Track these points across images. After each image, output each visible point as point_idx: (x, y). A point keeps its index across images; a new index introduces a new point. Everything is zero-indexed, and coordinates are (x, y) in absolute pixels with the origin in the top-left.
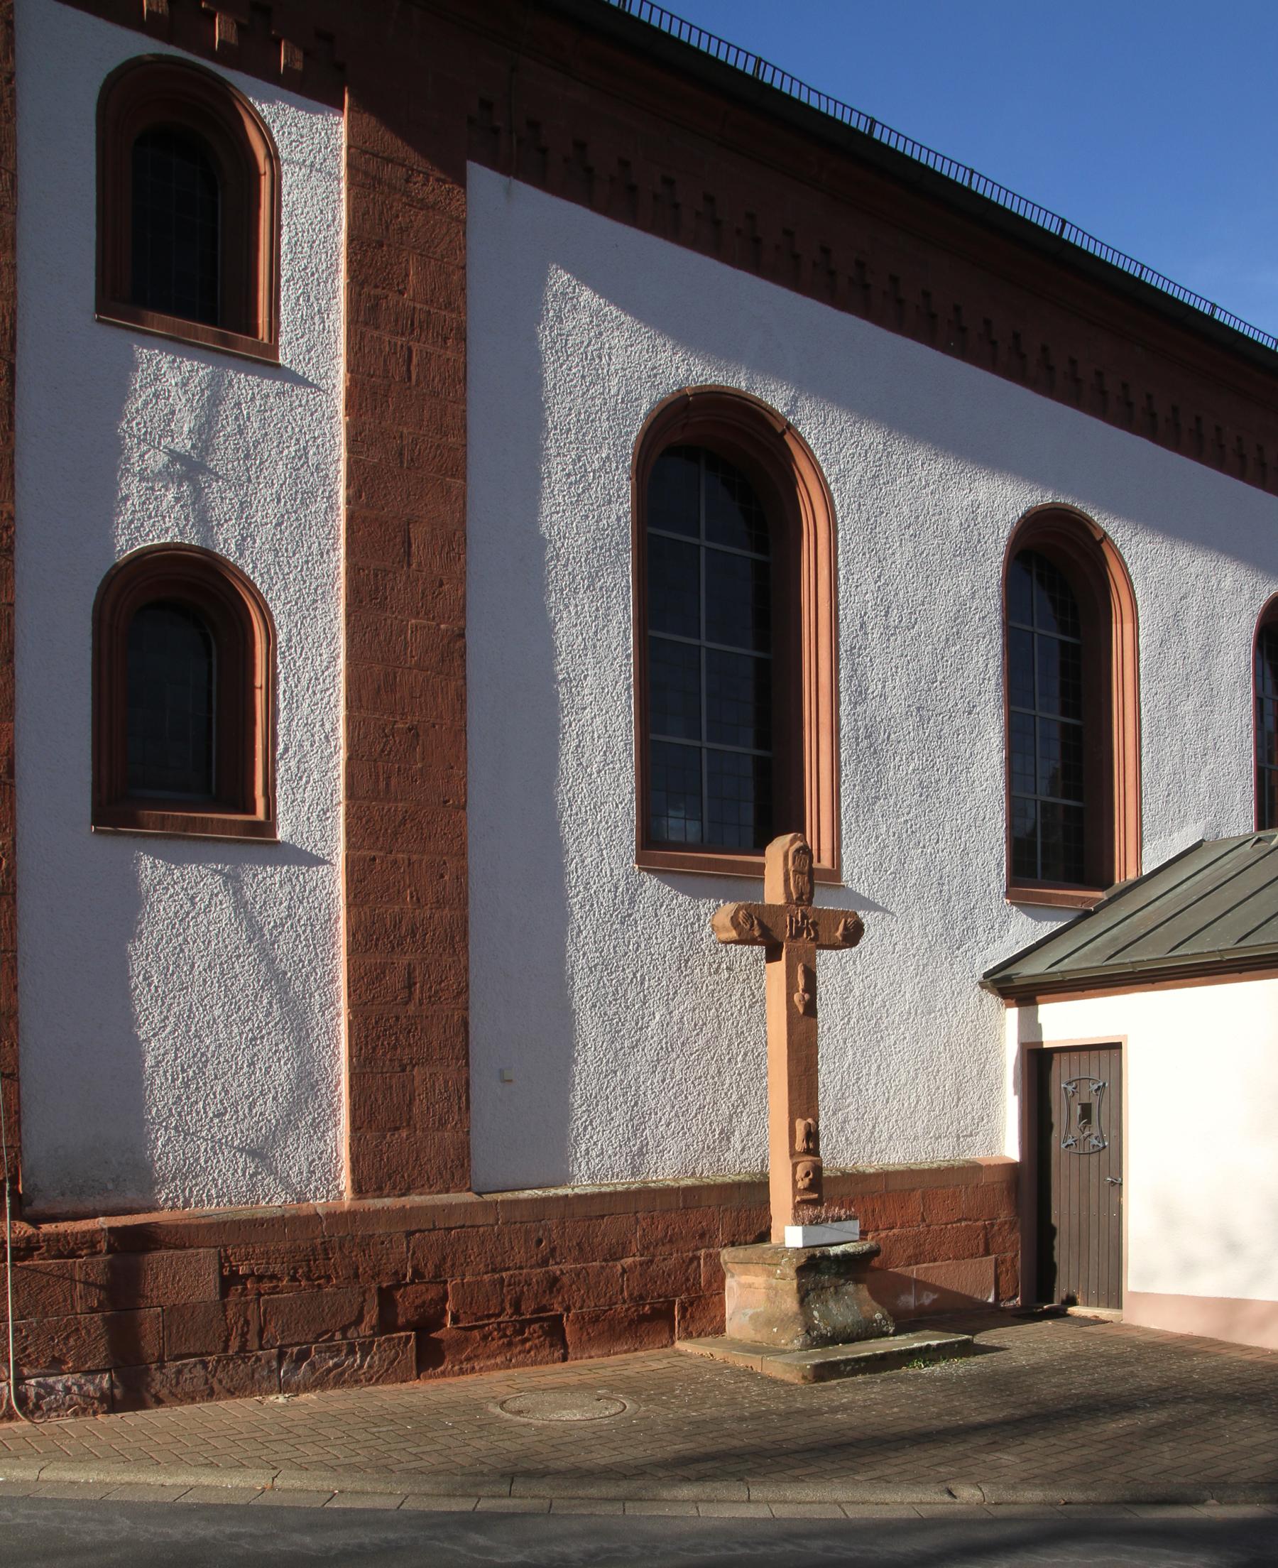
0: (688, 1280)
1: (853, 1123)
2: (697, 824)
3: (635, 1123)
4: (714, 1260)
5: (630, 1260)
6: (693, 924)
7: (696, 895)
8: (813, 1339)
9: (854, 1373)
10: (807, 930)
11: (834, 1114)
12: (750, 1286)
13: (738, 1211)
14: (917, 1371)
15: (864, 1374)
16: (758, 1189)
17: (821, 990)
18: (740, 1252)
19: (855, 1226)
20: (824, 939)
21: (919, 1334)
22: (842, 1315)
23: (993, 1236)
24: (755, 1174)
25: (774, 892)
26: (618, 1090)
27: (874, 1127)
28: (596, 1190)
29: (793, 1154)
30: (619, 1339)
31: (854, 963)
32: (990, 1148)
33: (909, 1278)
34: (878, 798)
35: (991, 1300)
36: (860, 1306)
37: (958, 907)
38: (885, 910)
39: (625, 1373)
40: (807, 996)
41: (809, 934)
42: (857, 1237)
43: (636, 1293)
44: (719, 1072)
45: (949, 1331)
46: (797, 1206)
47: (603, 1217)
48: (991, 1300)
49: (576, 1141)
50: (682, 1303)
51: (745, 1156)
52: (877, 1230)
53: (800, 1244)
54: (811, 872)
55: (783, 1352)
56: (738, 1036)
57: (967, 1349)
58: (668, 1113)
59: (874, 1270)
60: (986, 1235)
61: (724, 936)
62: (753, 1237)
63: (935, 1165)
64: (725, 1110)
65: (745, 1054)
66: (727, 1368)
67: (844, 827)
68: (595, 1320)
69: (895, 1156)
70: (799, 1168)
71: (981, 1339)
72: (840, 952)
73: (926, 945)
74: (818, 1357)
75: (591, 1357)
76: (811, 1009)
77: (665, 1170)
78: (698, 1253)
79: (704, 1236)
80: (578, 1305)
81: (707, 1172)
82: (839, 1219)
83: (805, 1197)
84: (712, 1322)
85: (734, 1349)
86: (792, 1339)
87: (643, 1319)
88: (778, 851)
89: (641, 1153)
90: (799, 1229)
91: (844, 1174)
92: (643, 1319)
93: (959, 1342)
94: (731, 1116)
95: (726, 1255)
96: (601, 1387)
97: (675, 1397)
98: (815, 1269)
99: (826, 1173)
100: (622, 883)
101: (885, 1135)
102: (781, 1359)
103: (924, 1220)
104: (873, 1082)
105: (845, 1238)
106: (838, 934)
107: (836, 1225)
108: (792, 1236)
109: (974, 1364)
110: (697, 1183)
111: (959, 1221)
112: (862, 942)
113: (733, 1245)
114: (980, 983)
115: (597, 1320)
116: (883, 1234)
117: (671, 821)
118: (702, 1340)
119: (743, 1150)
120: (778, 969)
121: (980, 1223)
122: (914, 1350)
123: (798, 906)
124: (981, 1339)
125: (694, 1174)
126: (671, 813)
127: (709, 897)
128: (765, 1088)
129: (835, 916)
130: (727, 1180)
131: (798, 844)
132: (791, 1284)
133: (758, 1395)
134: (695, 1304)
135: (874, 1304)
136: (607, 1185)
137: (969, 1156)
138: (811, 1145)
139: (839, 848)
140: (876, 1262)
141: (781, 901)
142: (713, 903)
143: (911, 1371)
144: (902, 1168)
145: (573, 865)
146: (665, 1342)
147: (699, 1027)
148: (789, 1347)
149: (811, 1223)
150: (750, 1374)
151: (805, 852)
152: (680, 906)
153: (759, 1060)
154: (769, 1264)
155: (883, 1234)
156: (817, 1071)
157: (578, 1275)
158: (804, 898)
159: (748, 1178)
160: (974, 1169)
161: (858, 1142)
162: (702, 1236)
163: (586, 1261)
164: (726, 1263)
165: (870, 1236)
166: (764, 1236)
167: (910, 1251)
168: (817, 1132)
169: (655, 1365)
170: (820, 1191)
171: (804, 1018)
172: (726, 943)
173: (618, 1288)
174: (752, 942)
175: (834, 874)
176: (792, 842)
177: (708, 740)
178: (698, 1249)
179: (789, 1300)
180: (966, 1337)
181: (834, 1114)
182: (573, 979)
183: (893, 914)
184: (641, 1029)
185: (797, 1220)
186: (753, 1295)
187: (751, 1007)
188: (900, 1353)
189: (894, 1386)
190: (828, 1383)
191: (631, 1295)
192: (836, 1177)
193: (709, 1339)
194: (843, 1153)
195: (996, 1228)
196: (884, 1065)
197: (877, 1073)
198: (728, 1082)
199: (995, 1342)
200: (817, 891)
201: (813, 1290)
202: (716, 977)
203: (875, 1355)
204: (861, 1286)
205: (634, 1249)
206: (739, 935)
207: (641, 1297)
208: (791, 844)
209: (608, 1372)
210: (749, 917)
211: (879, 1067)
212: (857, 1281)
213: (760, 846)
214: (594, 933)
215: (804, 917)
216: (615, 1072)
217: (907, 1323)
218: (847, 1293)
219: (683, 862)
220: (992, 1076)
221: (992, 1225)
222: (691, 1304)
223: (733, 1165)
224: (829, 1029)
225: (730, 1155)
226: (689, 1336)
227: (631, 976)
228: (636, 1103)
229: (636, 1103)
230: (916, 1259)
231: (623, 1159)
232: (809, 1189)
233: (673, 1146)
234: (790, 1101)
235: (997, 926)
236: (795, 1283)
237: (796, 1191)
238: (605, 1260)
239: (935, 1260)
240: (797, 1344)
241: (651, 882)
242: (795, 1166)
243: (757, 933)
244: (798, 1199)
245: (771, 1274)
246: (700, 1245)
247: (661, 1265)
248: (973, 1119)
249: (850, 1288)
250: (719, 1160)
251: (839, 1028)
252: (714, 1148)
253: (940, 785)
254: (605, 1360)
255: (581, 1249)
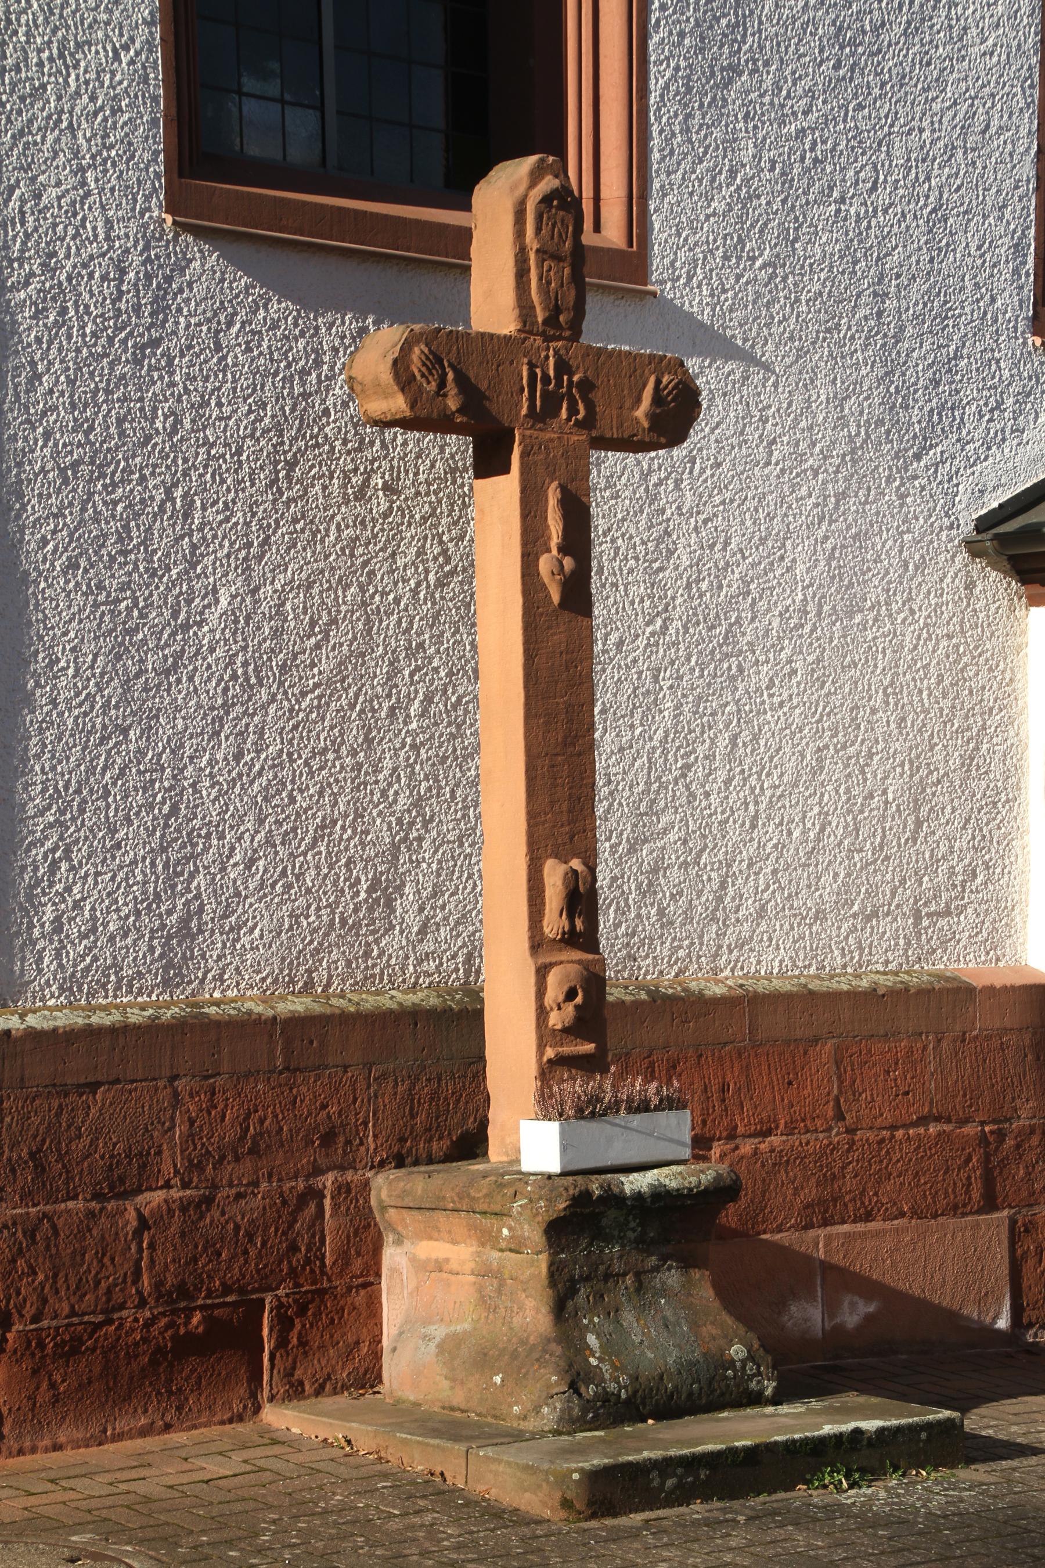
0: (294, 1248)
1: (675, 874)
2: (312, 117)
3: (173, 857)
4: (355, 1199)
5: (157, 1197)
6: (304, 372)
7: (311, 301)
8: (587, 1405)
9: (683, 1496)
10: (565, 401)
11: (632, 850)
12: (439, 1266)
13: (419, 1078)
14: (831, 1496)
15: (706, 1498)
16: (455, 1026)
17: (601, 550)
18: (417, 1182)
19: (678, 1126)
20: (607, 427)
21: (834, 1401)
22: (653, 1347)
23: (1003, 1163)
24: (452, 991)
25: (492, 303)
26: (133, 777)
27: (723, 885)
28: (79, 1020)
29: (537, 943)
30: (127, 1398)
32: (993, 945)
33: (808, 1259)
34: (735, 70)
35: (1003, 1323)
36: (694, 1326)
37: (919, 354)
38: (748, 358)
39: (140, 1487)
40: (568, 563)
41: (573, 411)
42: (686, 1153)
43: (170, 1281)
44: (369, 741)
45: (904, 1397)
46: (547, 1071)
47: (93, 1087)
48: (1003, 1323)
49: (30, 897)
50: (279, 1307)
51: (428, 946)
52: (732, 1136)
53: (555, 1168)
54: (579, 252)
55: (517, 1437)
56: (411, 653)
57: (949, 1447)
58: (250, 837)
59: (728, 1235)
60: (987, 1159)
61: (378, 407)
62: (446, 1143)
63: (864, 983)
64: (381, 831)
65: (428, 699)
66: (385, 1476)
67: (656, 142)
68: (71, 1349)
69: (769, 954)
70: (553, 978)
71: (984, 1421)
72: (645, 458)
73: (843, 448)
74: (598, 1451)
75: (57, 1447)
76: (577, 595)
77: (244, 976)
78: (319, 1182)
79: (333, 1140)
80: (29, 1311)
81: (343, 983)
82: (644, 1107)
83: (567, 1050)
84: (349, 1355)
85: (400, 1426)
86: (535, 1402)
87: (188, 1346)
88: (500, 201)
89: (186, 932)
90: (553, 1128)
91: (655, 995)
92: (188, 1346)
93: (929, 1426)
94: (395, 848)
95: (385, 1187)
96: (79, 1527)
97: (259, 1552)
98: (594, 1231)
99: (614, 994)
100: (135, 259)
101: (749, 907)
102: (512, 1454)
103: (840, 1116)
104: (722, 775)
105: (658, 1153)
106: (641, 412)
107: (637, 1120)
108: (536, 1145)
109: (970, 1483)
110: (317, 1009)
111: (923, 1121)
112: (695, 436)
113: (400, 1165)
114: (968, 543)
115: (75, 1351)
116: (747, 1147)
117: (250, 106)
118: (327, 1402)
119: (423, 931)
120: (500, 497)
121: (971, 1130)
122: (822, 1440)
123: (548, 339)
124: (984, 1421)
125: (309, 985)
126: (249, 84)
127: (341, 308)
128: (474, 783)
129: (636, 366)
130: (386, 1002)
131: (548, 183)
132: (534, 1265)
133: (458, 1547)
134: (304, 1313)
135: (729, 1320)
136: (104, 1008)
137: (945, 964)
138: (579, 924)
140: (730, 1216)
141: (506, 325)
142: (349, 323)
143: (817, 1497)
144: (786, 986)
145: (14, 204)
146: (237, 1407)
147: (321, 628)
148: (531, 1425)
149: (580, 1114)
150: (437, 1491)
151: (563, 205)
152: (275, 326)
153: (461, 714)
154: (483, 1212)
155: (747, 1147)
156: (591, 746)
157: (31, 1234)
158: (559, 318)
159: (434, 1001)
160: (957, 994)
161: (688, 919)
162: (328, 1139)
163: (52, 1198)
164: (384, 1208)
165: (715, 1152)
166: (472, 1144)
167: (810, 1192)
168: (593, 893)
169: (214, 1468)
170: (602, 1037)
171: (562, 613)
172: (384, 424)
173: (128, 1267)
174: (441, 424)
175: (633, 262)
176: (535, 176)
178: (318, 1171)
179: (530, 1303)
180: (946, 1414)
181: (632, 850)
182: (20, 496)
183: (767, 367)
184: (186, 627)
185: (548, 1106)
186: (445, 1288)
187: (440, 584)
188: (791, 1448)
189: (778, 1533)
190: (622, 1521)
191: (158, 1285)
192: (638, 1004)
193: (343, 1400)
194: (650, 949)
195: (1010, 1142)
196: (745, 736)
197: (730, 756)
198: (388, 764)
199: (1016, 1433)
200: (593, 303)
201: (587, 1279)
203: (733, 1451)
204: (696, 1274)
205: (167, 1169)
206: (413, 406)
207: (183, 1291)
208: (533, 183)
209: (97, 1486)
210: (434, 361)
211: (734, 739)
212: (687, 1263)
213: (459, 190)
214: (71, 382)
215: (563, 367)
216: (125, 732)
217: (807, 1373)
218: (664, 1291)
219: (280, 215)
220: (996, 769)
221: (1001, 1135)
222: (302, 1310)
223: (399, 972)
224: (620, 644)
225: (393, 943)
226: (295, 1392)
227: (159, 495)
228: (174, 810)
229: (174, 810)
230: (823, 1212)
232: (575, 1030)
233: (262, 918)
234: (532, 816)
235: (1009, 402)
236: (543, 1259)
237: (544, 1035)
238: (97, 1196)
239: (868, 1217)
240: (549, 1415)
241: (204, 262)
242: (542, 972)
244: (550, 1053)
245: (488, 1239)
246: (322, 1162)
247: (233, 1210)
248: (952, 873)
249: (672, 1277)
250: (367, 954)
251: (641, 642)
252: (357, 925)
253: (885, 38)
254: (92, 1454)
255: (40, 1169)
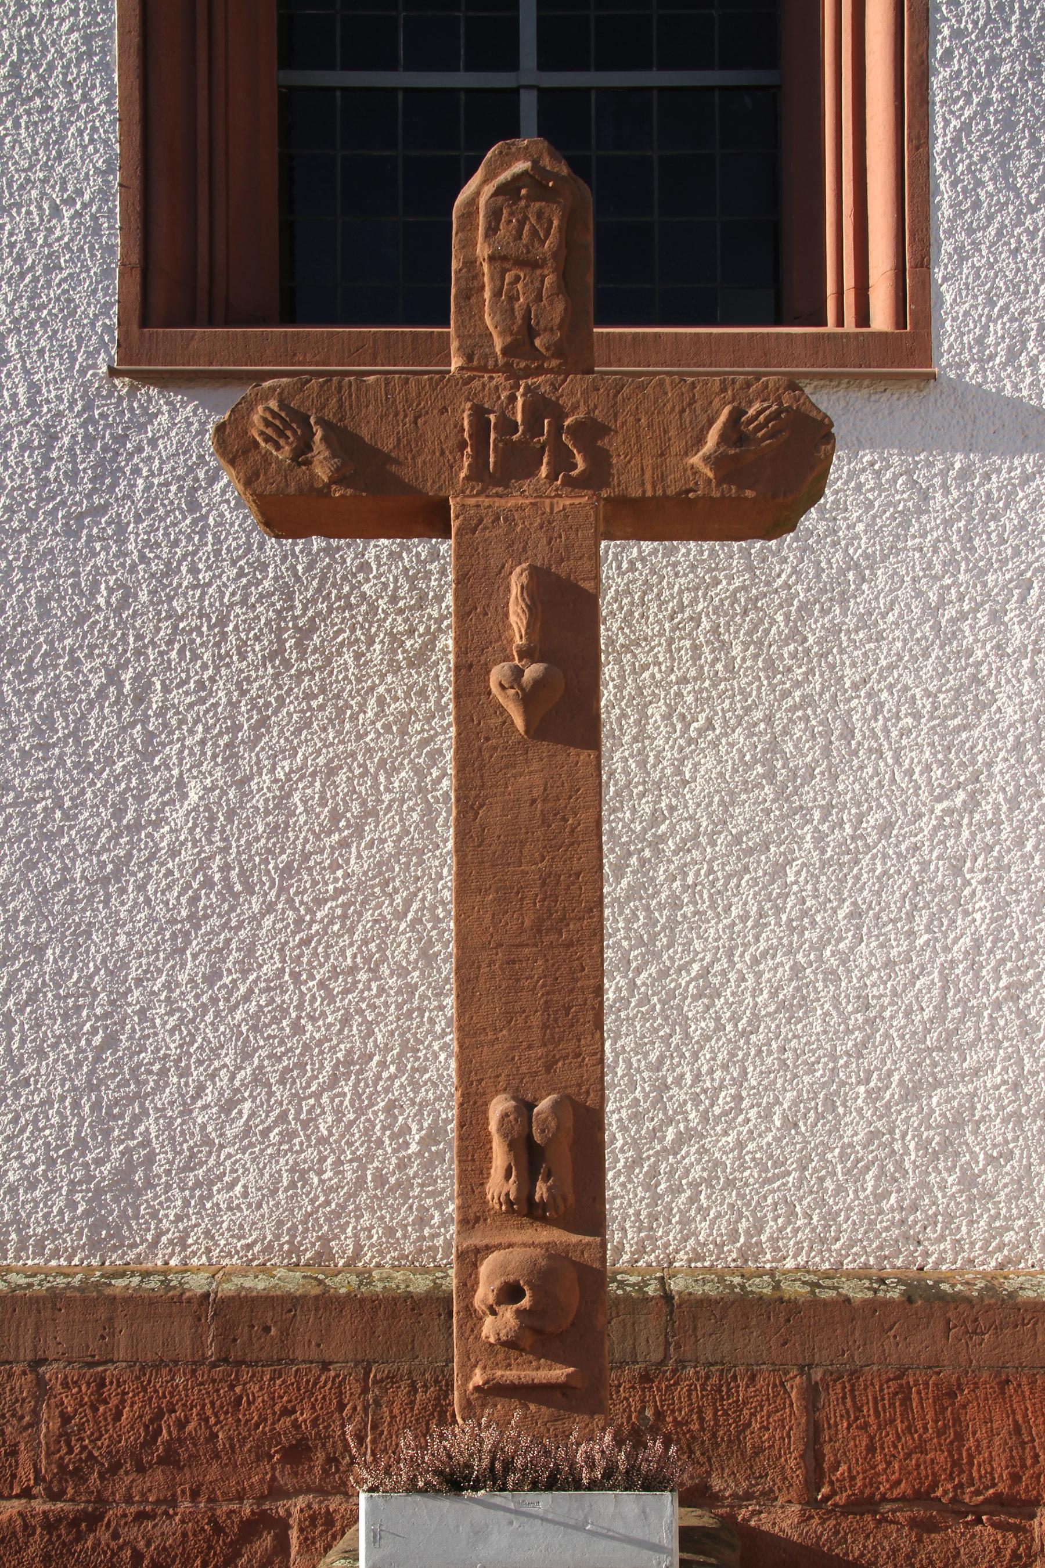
3: (107, 1096)
31: (995, 617)
123: (515, 377)
139: (924, 264)
162: (297, 1453)
177: (544, 65)
178: (276, 1492)
184: (135, 827)
194: (676, 1213)
202: (416, 677)
205: (25, 1473)
216: (40, 951)
224: (885, 828)
228: (111, 1041)
231: (59, 1202)
243: (322, 470)
246: (285, 1480)
251: (927, 824)
